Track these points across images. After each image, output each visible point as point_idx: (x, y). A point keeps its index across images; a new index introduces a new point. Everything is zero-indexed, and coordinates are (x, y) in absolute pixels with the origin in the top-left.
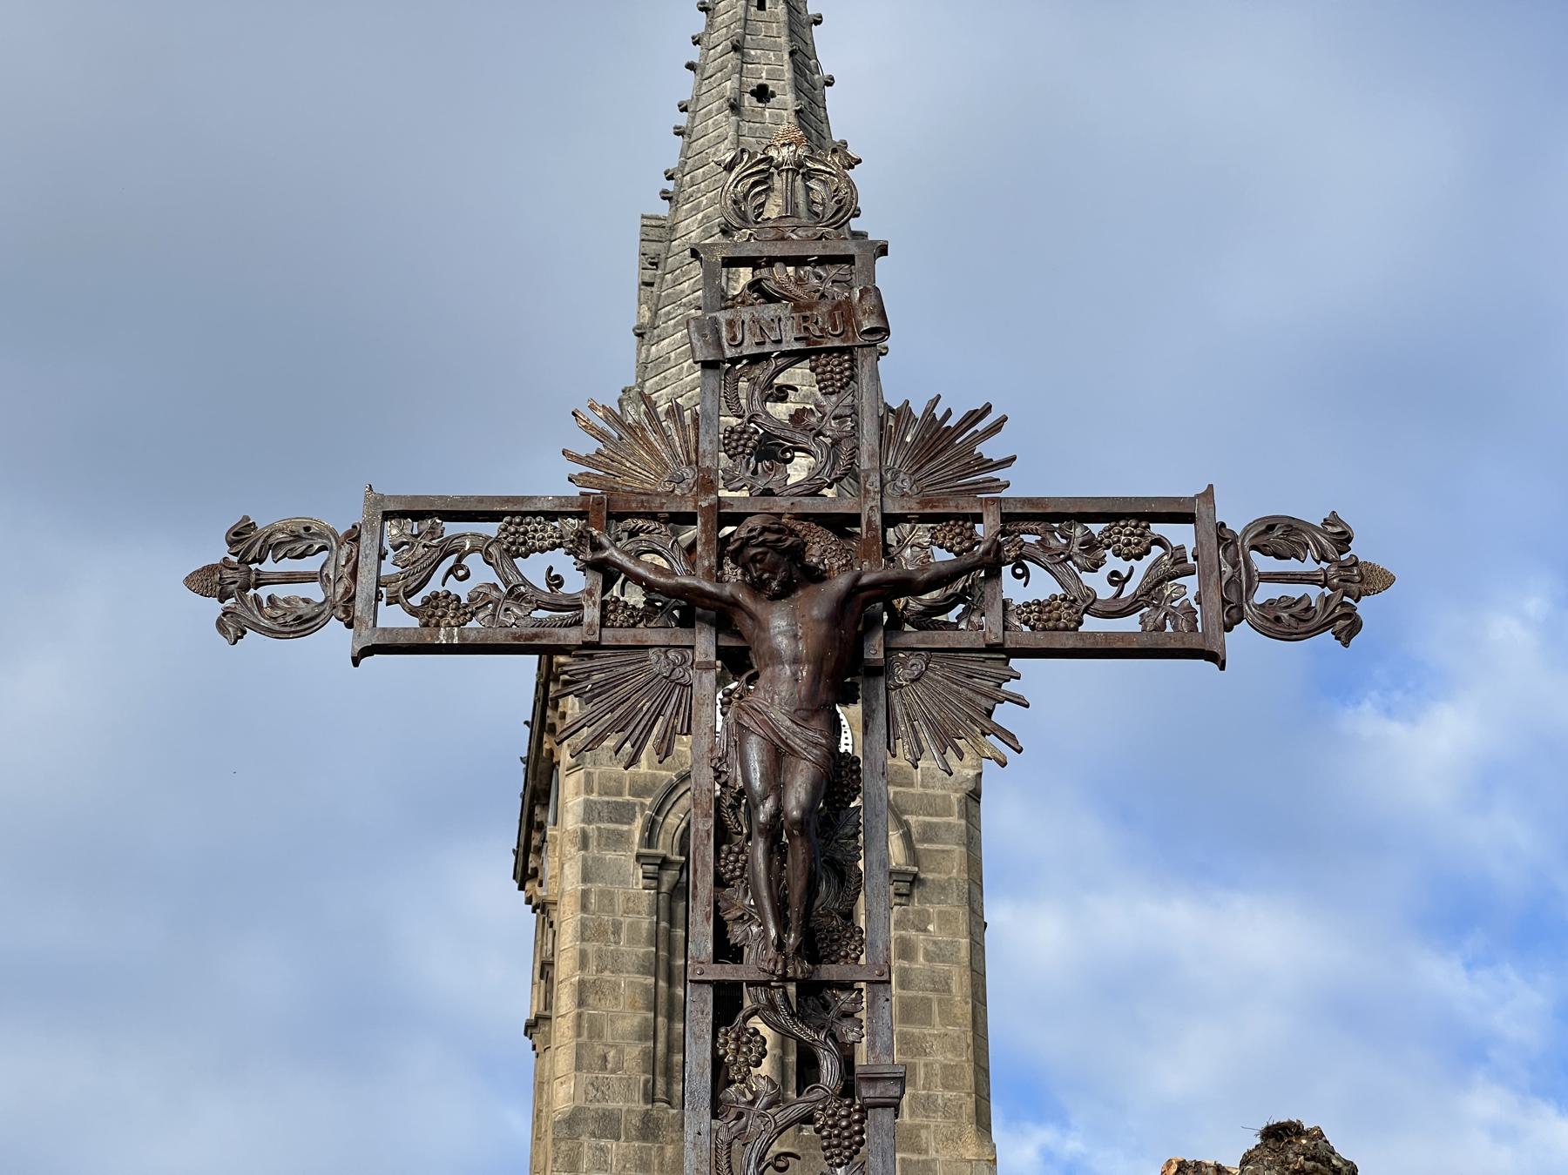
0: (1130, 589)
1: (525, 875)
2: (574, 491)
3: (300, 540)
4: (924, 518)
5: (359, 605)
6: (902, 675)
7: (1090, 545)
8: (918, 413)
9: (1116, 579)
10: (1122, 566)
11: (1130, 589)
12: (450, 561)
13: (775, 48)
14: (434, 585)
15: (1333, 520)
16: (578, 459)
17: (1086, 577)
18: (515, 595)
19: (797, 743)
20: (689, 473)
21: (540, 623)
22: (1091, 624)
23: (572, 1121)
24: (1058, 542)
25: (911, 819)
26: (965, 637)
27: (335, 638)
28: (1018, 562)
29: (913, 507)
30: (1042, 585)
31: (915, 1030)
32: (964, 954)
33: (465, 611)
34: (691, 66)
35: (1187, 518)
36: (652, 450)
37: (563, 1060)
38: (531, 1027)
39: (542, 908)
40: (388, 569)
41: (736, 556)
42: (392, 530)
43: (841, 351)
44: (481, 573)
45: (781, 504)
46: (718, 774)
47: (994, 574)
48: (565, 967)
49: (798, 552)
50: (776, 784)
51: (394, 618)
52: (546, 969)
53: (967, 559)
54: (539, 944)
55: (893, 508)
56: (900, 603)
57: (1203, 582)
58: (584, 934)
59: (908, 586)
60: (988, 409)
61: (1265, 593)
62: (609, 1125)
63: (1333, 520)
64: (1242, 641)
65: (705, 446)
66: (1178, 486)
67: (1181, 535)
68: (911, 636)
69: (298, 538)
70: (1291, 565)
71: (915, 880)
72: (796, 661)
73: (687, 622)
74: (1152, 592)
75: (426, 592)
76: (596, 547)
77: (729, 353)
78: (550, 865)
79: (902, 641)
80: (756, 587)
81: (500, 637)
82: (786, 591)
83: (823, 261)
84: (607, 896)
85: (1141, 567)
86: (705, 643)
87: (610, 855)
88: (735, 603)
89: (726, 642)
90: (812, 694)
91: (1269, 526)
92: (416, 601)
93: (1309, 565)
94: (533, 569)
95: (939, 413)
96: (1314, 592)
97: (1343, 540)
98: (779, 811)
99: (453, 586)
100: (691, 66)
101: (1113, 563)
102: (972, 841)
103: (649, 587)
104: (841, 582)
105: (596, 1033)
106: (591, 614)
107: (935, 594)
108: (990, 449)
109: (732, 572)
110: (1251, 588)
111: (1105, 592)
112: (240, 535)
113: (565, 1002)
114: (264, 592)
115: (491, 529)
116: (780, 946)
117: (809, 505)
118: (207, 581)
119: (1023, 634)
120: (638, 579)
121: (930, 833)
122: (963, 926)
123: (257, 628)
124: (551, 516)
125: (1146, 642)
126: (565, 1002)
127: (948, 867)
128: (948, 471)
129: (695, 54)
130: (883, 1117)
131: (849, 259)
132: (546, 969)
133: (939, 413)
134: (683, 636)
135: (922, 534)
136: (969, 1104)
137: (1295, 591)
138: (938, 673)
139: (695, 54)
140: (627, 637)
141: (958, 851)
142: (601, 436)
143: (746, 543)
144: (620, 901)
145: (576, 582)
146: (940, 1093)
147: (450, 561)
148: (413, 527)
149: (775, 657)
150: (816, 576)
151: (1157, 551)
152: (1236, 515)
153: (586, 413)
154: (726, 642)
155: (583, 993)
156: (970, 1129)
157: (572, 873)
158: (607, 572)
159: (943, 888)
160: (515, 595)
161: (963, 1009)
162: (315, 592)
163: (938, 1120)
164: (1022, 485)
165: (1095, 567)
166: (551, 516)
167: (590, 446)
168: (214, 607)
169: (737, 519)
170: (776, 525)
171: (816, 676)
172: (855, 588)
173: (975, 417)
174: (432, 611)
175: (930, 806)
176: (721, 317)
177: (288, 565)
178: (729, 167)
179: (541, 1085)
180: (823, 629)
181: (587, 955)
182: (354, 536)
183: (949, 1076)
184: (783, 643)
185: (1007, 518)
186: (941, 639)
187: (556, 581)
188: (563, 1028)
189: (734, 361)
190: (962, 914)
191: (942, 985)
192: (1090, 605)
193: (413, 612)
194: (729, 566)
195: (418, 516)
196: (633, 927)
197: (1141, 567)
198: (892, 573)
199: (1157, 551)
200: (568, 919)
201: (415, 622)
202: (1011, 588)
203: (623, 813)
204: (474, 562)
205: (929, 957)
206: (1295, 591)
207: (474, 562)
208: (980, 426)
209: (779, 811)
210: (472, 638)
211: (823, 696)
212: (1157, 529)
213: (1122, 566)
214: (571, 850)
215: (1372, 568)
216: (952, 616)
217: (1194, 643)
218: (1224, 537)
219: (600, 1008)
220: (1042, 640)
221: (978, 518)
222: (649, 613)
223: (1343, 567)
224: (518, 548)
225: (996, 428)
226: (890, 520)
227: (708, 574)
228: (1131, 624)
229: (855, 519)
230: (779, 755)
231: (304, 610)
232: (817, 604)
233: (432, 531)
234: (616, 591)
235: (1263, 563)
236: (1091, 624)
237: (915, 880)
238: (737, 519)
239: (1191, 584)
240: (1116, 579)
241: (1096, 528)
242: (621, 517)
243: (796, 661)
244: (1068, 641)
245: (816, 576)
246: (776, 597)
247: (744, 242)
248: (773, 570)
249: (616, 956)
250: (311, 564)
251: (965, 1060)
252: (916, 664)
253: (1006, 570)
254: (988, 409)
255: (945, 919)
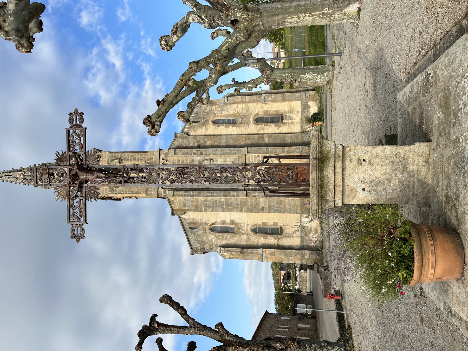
0: (78, 138)
1: (120, 200)
2: (66, 200)
3: (73, 231)
4: (69, 161)
5: (80, 224)
6: (88, 163)
7: (72, 142)
8: (56, 161)
9: (77, 139)
10: (75, 139)
11: (78, 138)
12: (75, 214)
13: (17, 174)
14: (78, 215)
15: (69, 114)
16: (62, 200)
17: (76, 143)
18: (79, 206)
19: (96, 175)
20: (64, 187)
21: (83, 203)
22: (82, 142)
23: (146, 194)
24: (72, 146)
25: (113, 159)
26: (84, 156)
27: (85, 226)
28: (74, 150)
29: (68, 162)
30: (77, 147)
31: (137, 159)
32: (128, 154)
33: (81, 212)
34: (19, 184)
35: (69, 131)
36: (61, 191)
37: (140, 195)
38: (137, 198)
39: (124, 198)
40: (76, 221)
41: (74, 182)
42: (71, 220)
43: (48, 170)
44: (77, 210)
45: (68, 177)
46: (100, 184)
47: (76, 153)
48: (130, 195)
49: (73, 175)
50: (101, 177)
51: (82, 220)
52: (130, 197)
53: (74, 156)
54: (128, 198)
55: (68, 164)
56: (80, 164)
57: (77, 130)
58: (126, 193)
59: (77, 163)
60: (56, 153)
61: (78, 123)
62: (147, 190)
63: (69, 114)
64: (84, 125)
65: (61, 185)
66: (65, 131)
67: (71, 132)
68: (83, 162)
69: (72, 231)
70: (75, 120)
71: (120, 159)
72: (86, 175)
73: (82, 187)
74: (78, 135)
75: (79, 216)
76: (73, 197)
77: (49, 183)
78: (119, 197)
79: (84, 164)
80: (78, 180)
81: (84, 208)
82: (78, 176)
83: (36, 172)
84: (122, 191)
85: (75, 136)
86: (85, 185)
87: (118, 191)
88: (80, 182)
89: (85, 183)
90: (90, 173)
91: (70, 122)
92: (80, 217)
93: (75, 117)
94: (76, 204)
95: (56, 159)
96: (78, 117)
97: (71, 114)
98: (104, 177)
99: (78, 213)
100: (19, 184)
101: (75, 140)
102: (116, 153)
103: (78, 191)
104: (77, 170)
105: (137, 192)
106: (81, 198)
107: (78, 160)
108: (61, 153)
109: (76, 182)
110: (78, 124)
111: (78, 141)
112: (72, 237)
113: (134, 195)
114: (79, 234)
115: (71, 209)
116: (120, 177)
117: (68, 174)
118: (78, 240)
119: (83, 150)
120: (77, 193)
121: (115, 157)
122: (125, 154)
123: (83, 235)
124: (70, 203)
125: (84, 136)
126: (134, 195)
127: (118, 155)
128: (64, 158)
129: (18, 183)
130: (138, 166)
131: (36, 169)
132: (130, 197)
133: (56, 159)
134: (84, 188)
135: (71, 161)
136: (144, 153)
137: (78, 119)
138: (88, 160)
139: (18, 183)
140: (84, 194)
141: (117, 154)
142: (59, 197)
143: (72, 181)
144: (123, 190)
145: (78, 199)
146: (143, 156)
147: (75, 214)
148: (71, 218)
149: (86, 178)
150: (76, 173)
151: (73, 135)
152: (69, 125)
153: (57, 199)
154: (85, 183)
155: (133, 193)
156: (147, 153)
157: (120, 195)
158: (76, 196)
159: (121, 156)
160: (79, 206)
161: (134, 154)
162: (79, 229)
163: (146, 157)
164: (65, 150)
165: (75, 142)
166: (70, 203)
167: (61, 199)
168: (81, 240)
169: (70, 182)
170: (70, 177)
171: (88, 173)
172: (78, 169)
173: (57, 155)
174: (81, 216)
175: (112, 157)
176: (44, 184)
177: (76, 232)
178: (24, 183)
179: (143, 197)
180: (83, 172)
181: (261, 114)
182: (72, 225)
183: (141, 155)
184: (84, 177)
185: (69, 151)
186: (84, 159)
187: (78, 202)
188: (137, 195)
189: (50, 182)
190: (124, 154)
191: (132, 156)
192: (80, 143)
193: (81, 218)
194: (75, 183)
195: (70, 218)
196: (125, 188)
197: (75, 136)
198: (76, 165)
199: (73, 135)
200: (125, 195)
201: (83, 217)
202: (78, 151)
203: (113, 190)
204: (75, 211)
205: (129, 157)
206: (78, 119)
207: (75, 211)
208: (58, 154)
209: (104, 177)
210: (84, 211)
211: (90, 172)
212: (70, 135)
213: (75, 139)
214: (117, 195)
215: (75, 110)
216: (81, 158)
217: (84, 131)
218: (71, 127)
219: (134, 191)
220: (84, 148)
221: (69, 155)
222: (81, 192)
223: (75, 114)
224: (74, 206)
225: (58, 152)
226: (70, 164)
227: (76, 185)
228: (82, 138)
229: (70, 169)
230: (98, 177)
231: (81, 230)
232: (80, 173)
233: (71, 216)
234: (79, 195)
235: (74, 123)
236: (82, 142)
237: (120, 159)
238: (70, 182)
239: (77, 131)
240: (77, 139)
241: (70, 141)
242: (70, 195)
243: (86, 175)
244: (84, 145)
245: (76, 173)
246: (79, 178)
247: (34, 182)
248: (75, 178)
249: (129, 190)
250: (76, 229)
251: (140, 154)
252: (87, 162)
253: (76, 152)
254: (56, 153)
255: (124, 155)
